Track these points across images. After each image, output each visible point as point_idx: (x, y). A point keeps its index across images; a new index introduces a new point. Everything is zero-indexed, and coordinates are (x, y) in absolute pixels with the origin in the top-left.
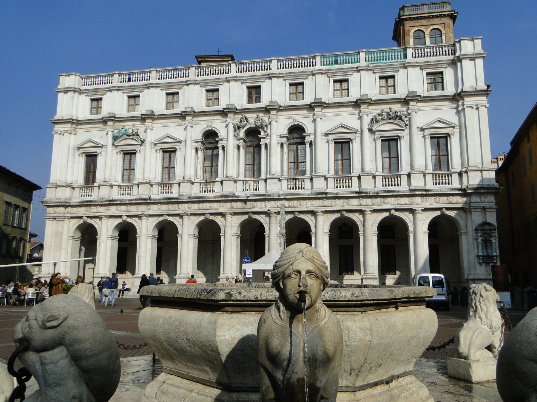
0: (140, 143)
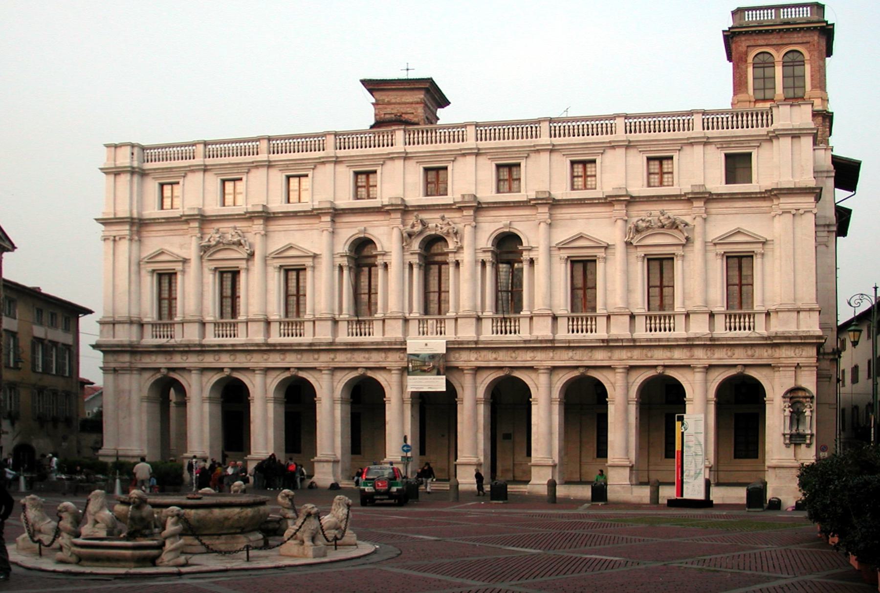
0: (684, 241)
